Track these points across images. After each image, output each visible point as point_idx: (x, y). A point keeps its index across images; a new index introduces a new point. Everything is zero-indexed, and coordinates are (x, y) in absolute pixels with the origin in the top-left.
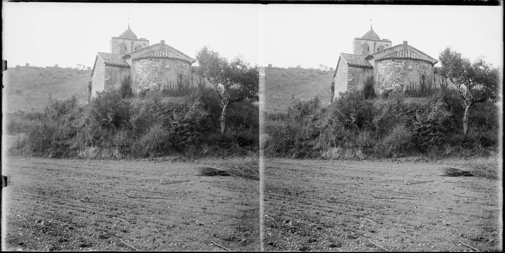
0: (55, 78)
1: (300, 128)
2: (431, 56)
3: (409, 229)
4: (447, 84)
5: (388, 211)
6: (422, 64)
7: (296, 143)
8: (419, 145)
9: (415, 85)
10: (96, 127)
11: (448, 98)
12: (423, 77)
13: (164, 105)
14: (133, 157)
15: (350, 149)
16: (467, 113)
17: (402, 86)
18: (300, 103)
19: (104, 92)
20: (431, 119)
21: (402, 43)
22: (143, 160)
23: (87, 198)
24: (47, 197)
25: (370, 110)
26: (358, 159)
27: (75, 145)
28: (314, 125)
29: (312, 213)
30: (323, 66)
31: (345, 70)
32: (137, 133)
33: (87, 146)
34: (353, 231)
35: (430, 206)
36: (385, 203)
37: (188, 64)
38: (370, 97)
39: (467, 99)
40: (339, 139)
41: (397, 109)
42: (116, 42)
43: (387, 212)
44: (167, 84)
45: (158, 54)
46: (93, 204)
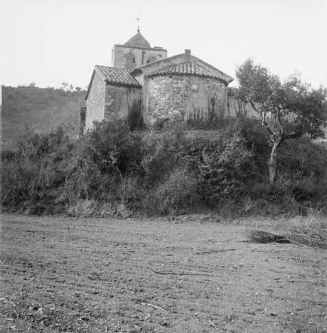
2: (223, 71)
3: (218, 321)
5: (180, 292)
6: (211, 82)
8: (206, 199)
9: (201, 112)
12: (213, 101)
13: (190, 142)
14: (145, 215)
15: (109, 202)
17: (183, 113)
18: (37, 136)
19: (104, 121)
20: (224, 161)
22: (159, 218)
24: (36, 271)
27: (62, 197)
28: (57, 167)
29: (70, 295)
30: (67, 85)
31: (102, 89)
33: (80, 198)
34: (137, 324)
35: (240, 286)
37: (223, 84)
38: (136, 128)
40: (94, 188)
41: (176, 145)
45: (181, 69)
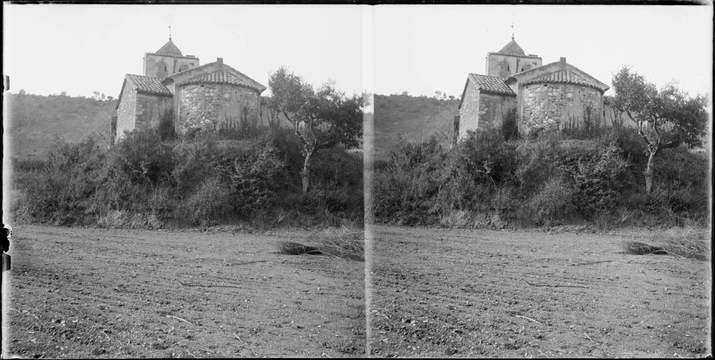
0: (403, 111)
1: (67, 182)
2: (256, 80)
4: (279, 121)
5: (555, 305)
6: (587, 91)
7: (60, 204)
8: (585, 208)
9: (576, 121)
10: (123, 182)
11: (624, 141)
12: (588, 110)
13: (565, 151)
14: (520, 226)
16: (308, 162)
17: (558, 122)
19: (135, 131)
21: (559, 60)
23: (122, 286)
25: (168, 156)
26: (151, 227)
31: (476, 97)
32: (525, 192)
36: (548, 293)
37: (255, 93)
38: (168, 138)
39: (651, 143)
40: (467, 198)
42: (152, 60)
43: (554, 308)
44: (226, 122)
45: (213, 78)
46: (133, 294)
